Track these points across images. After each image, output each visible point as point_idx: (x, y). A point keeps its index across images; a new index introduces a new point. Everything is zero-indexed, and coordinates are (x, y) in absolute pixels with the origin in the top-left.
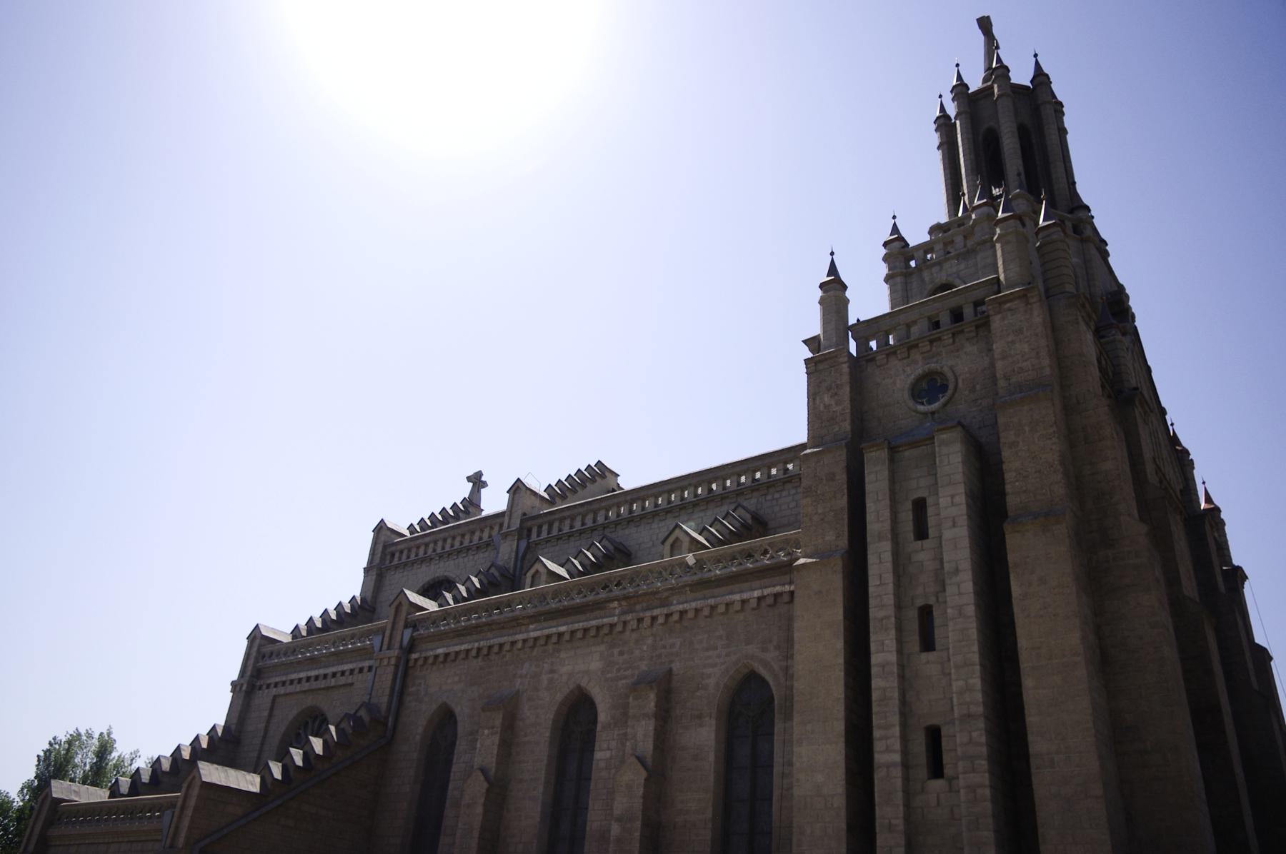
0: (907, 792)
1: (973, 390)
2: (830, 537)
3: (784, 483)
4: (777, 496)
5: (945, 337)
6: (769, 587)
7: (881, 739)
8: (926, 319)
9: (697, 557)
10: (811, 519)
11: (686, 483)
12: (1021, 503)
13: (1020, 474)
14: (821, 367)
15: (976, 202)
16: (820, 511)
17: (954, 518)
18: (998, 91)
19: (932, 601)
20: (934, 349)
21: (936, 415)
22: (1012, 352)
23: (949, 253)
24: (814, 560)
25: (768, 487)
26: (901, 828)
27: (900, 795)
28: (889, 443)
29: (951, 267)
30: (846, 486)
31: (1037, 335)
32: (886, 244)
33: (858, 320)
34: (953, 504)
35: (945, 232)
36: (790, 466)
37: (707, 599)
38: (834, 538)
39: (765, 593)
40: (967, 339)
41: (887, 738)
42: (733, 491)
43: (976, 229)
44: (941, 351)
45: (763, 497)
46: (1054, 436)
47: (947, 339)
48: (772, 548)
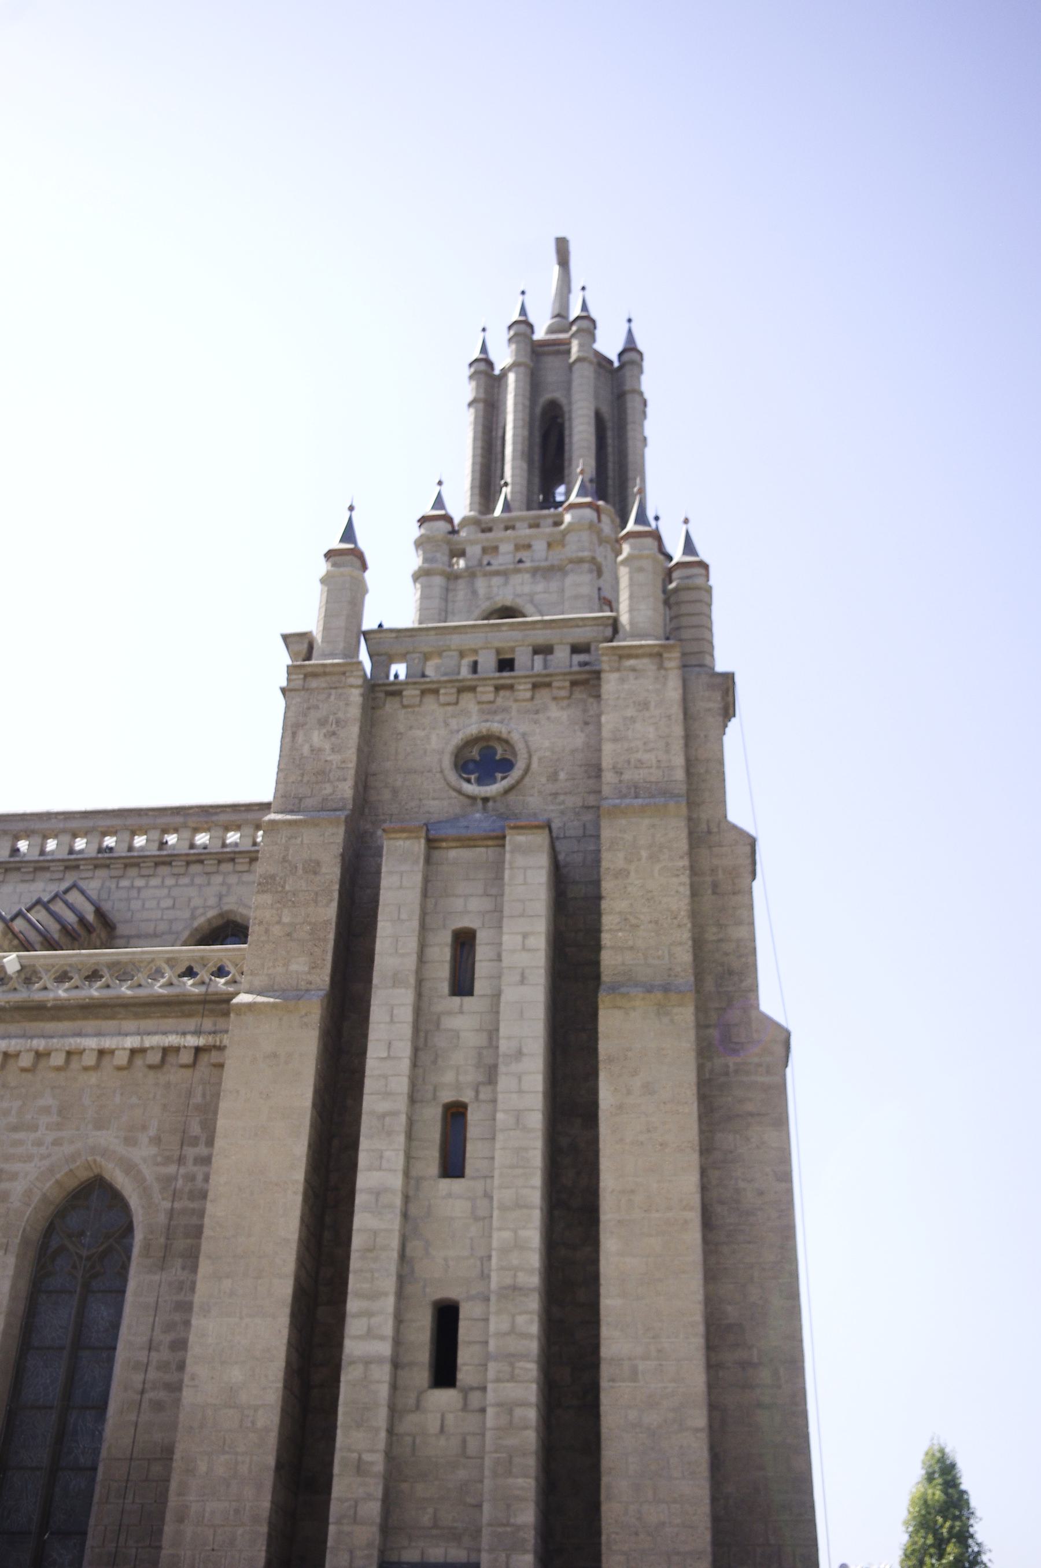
0: (394, 1411)
1: (553, 777)
2: (299, 966)
3: (157, 864)
4: (140, 883)
5: (522, 687)
6: (155, 1033)
7: (359, 1315)
8: (494, 651)
9: (25, 962)
10: (267, 931)
11: (144, 821)
12: (623, 964)
13: (626, 919)
14: (314, 683)
15: (573, 498)
16: (286, 919)
17: (523, 970)
18: (579, 351)
19: (467, 1097)
20: (499, 700)
21: (490, 804)
22: (630, 733)
23: (520, 561)
24: (272, 1000)
25: (126, 866)
26: (379, 1467)
27: (383, 1413)
28: (428, 830)
29: (522, 584)
30: (337, 887)
31: (669, 717)
32: (423, 520)
33: (380, 626)
34: (524, 949)
35: (483, 531)
36: (172, 839)
37: (32, 1037)
38: (306, 969)
39: (147, 1044)
40: (555, 699)
41: (369, 1314)
42: (59, 860)
43: (568, 538)
44: (511, 707)
45: (114, 881)
46: (683, 874)
47: (523, 690)
48: (172, 967)
